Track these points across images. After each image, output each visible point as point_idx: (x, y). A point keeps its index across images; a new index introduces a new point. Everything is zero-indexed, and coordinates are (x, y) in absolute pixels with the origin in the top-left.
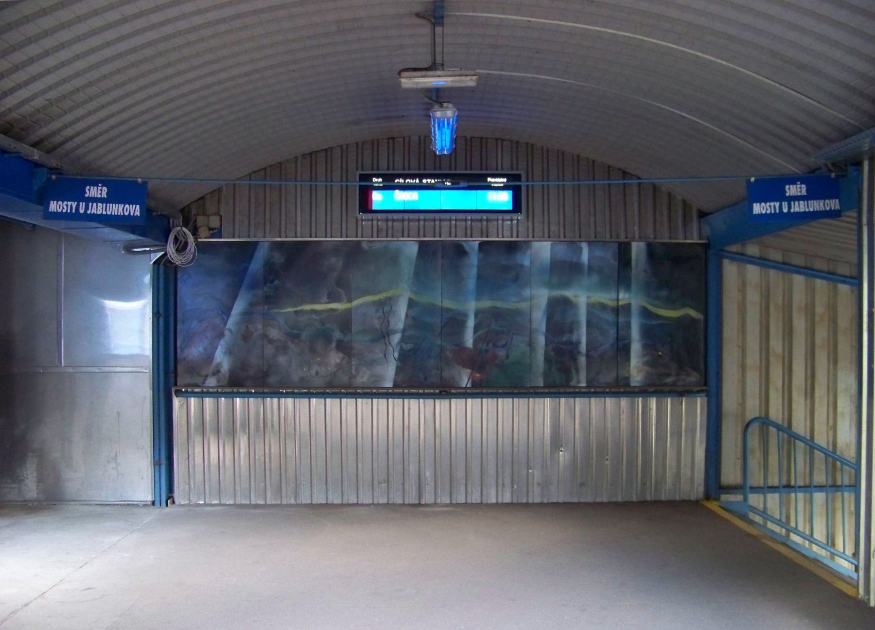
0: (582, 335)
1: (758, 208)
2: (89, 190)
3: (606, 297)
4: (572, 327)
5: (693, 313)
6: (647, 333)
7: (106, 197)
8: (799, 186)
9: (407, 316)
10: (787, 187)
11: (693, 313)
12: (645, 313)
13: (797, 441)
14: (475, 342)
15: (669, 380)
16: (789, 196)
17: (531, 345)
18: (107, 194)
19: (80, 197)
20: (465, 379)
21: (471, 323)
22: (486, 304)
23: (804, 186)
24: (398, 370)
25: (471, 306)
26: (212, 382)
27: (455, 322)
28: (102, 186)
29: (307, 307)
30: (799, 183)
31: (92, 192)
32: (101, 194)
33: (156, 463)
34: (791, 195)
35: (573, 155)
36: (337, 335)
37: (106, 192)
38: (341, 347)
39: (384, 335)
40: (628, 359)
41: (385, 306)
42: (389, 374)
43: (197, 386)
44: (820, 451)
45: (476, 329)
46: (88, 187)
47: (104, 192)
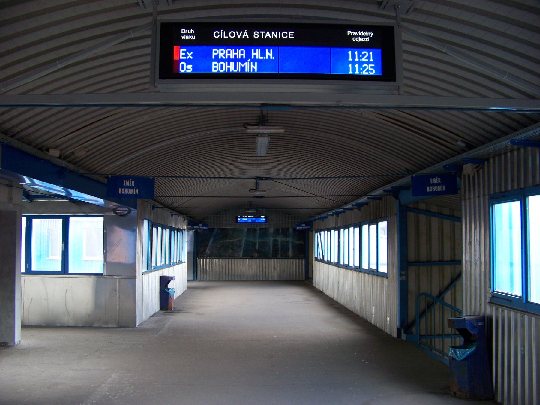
0: (280, 246)
1: (298, 228)
2: (125, 182)
3: (285, 239)
4: (278, 245)
5: (302, 242)
6: (293, 247)
7: (134, 185)
8: (437, 179)
9: (245, 243)
10: (431, 179)
11: (302, 242)
12: (292, 242)
13: (445, 306)
14: (259, 248)
15: (298, 256)
16: (432, 184)
17: (269, 248)
18: (134, 184)
19: (198, 226)
20: (256, 255)
21: (257, 244)
22: (260, 240)
23: (439, 179)
24: (243, 253)
25: (258, 241)
26: (205, 256)
27: (254, 244)
28: (132, 180)
29: (225, 241)
30: (437, 177)
31: (200, 225)
32: (131, 184)
33: (194, 272)
34: (433, 183)
35: (189, 288)
36: (231, 246)
37: (134, 183)
38: (232, 249)
39: (240, 246)
40: (289, 252)
41: (240, 241)
42: (241, 255)
43: (202, 256)
44: (448, 306)
45: (259, 245)
46: (125, 181)
47: (202, 225)
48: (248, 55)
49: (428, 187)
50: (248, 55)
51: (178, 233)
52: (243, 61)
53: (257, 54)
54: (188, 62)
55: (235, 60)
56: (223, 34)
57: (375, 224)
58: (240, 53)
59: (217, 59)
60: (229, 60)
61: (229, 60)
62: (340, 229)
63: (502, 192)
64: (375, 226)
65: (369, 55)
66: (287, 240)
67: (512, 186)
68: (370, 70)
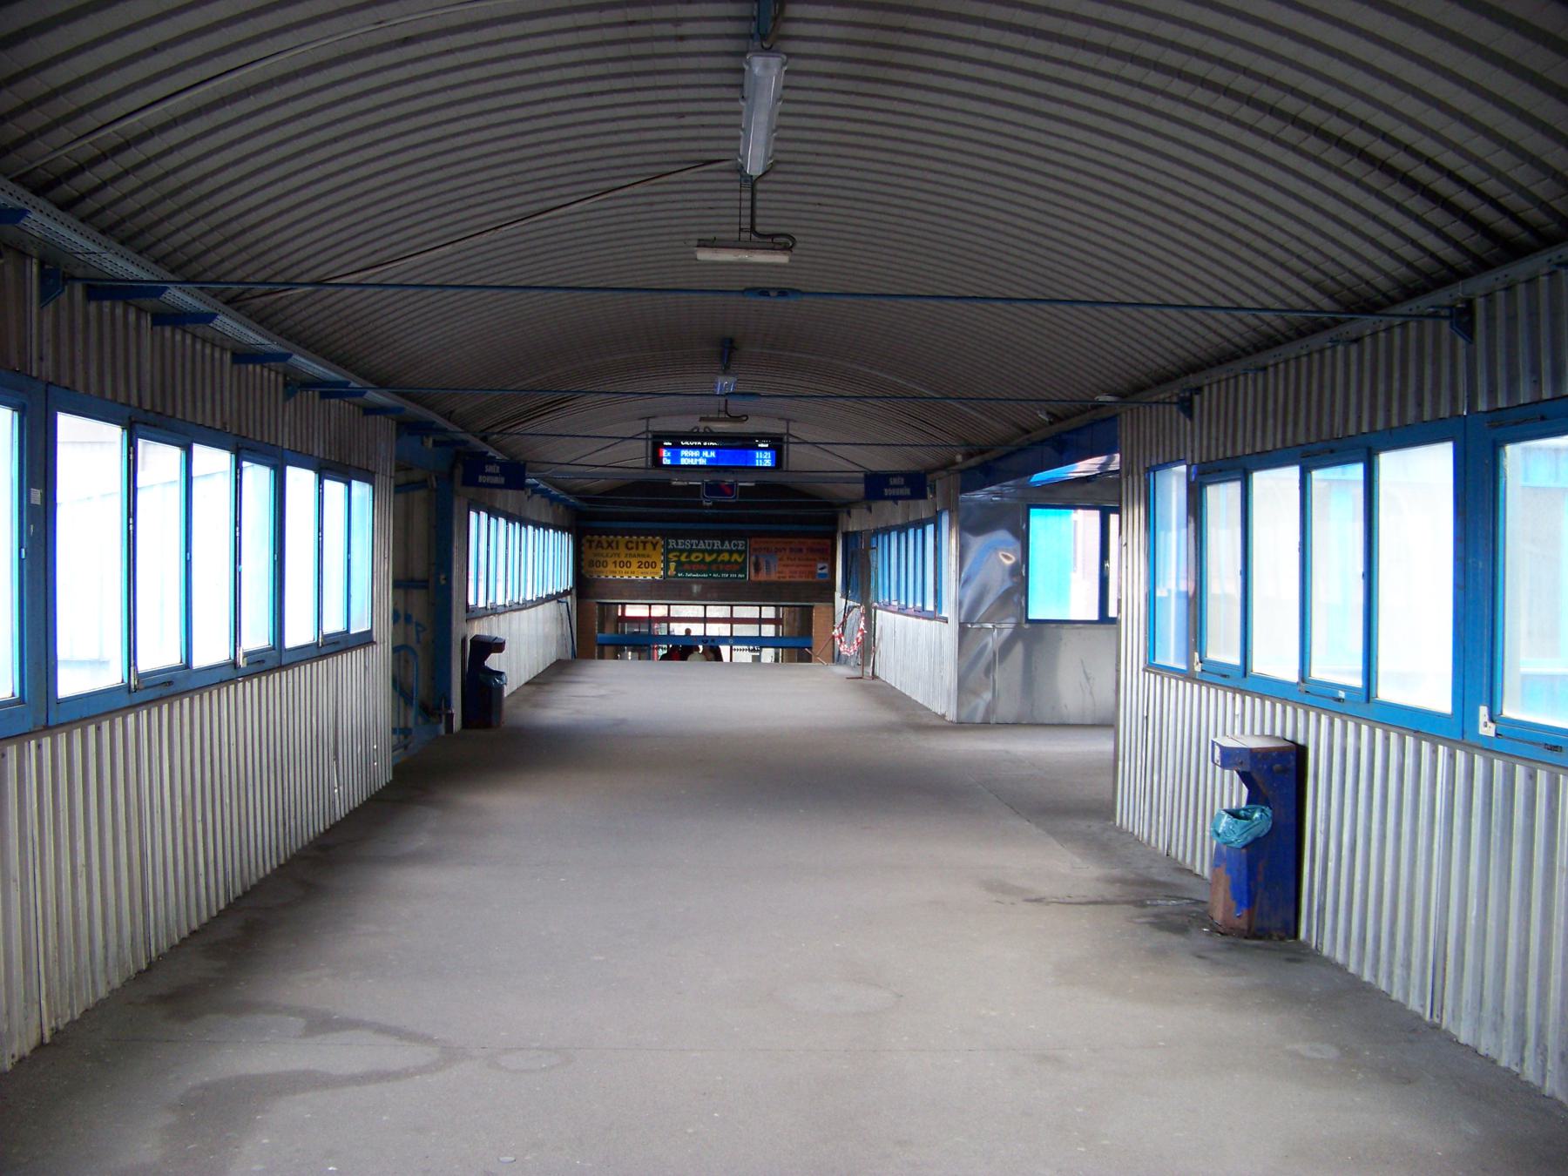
48: (701, 455)
49: (886, 490)
50: (701, 455)
51: (510, 525)
52: (698, 458)
53: (705, 453)
54: (668, 458)
55: (694, 457)
56: (687, 443)
57: (1234, 480)
58: (697, 453)
59: (684, 457)
60: (690, 457)
61: (690, 457)
62: (1503, 446)
63: (1322, 441)
64: (1356, 471)
65: (768, 454)
66: (813, 574)
67: (1372, 423)
68: (768, 463)
